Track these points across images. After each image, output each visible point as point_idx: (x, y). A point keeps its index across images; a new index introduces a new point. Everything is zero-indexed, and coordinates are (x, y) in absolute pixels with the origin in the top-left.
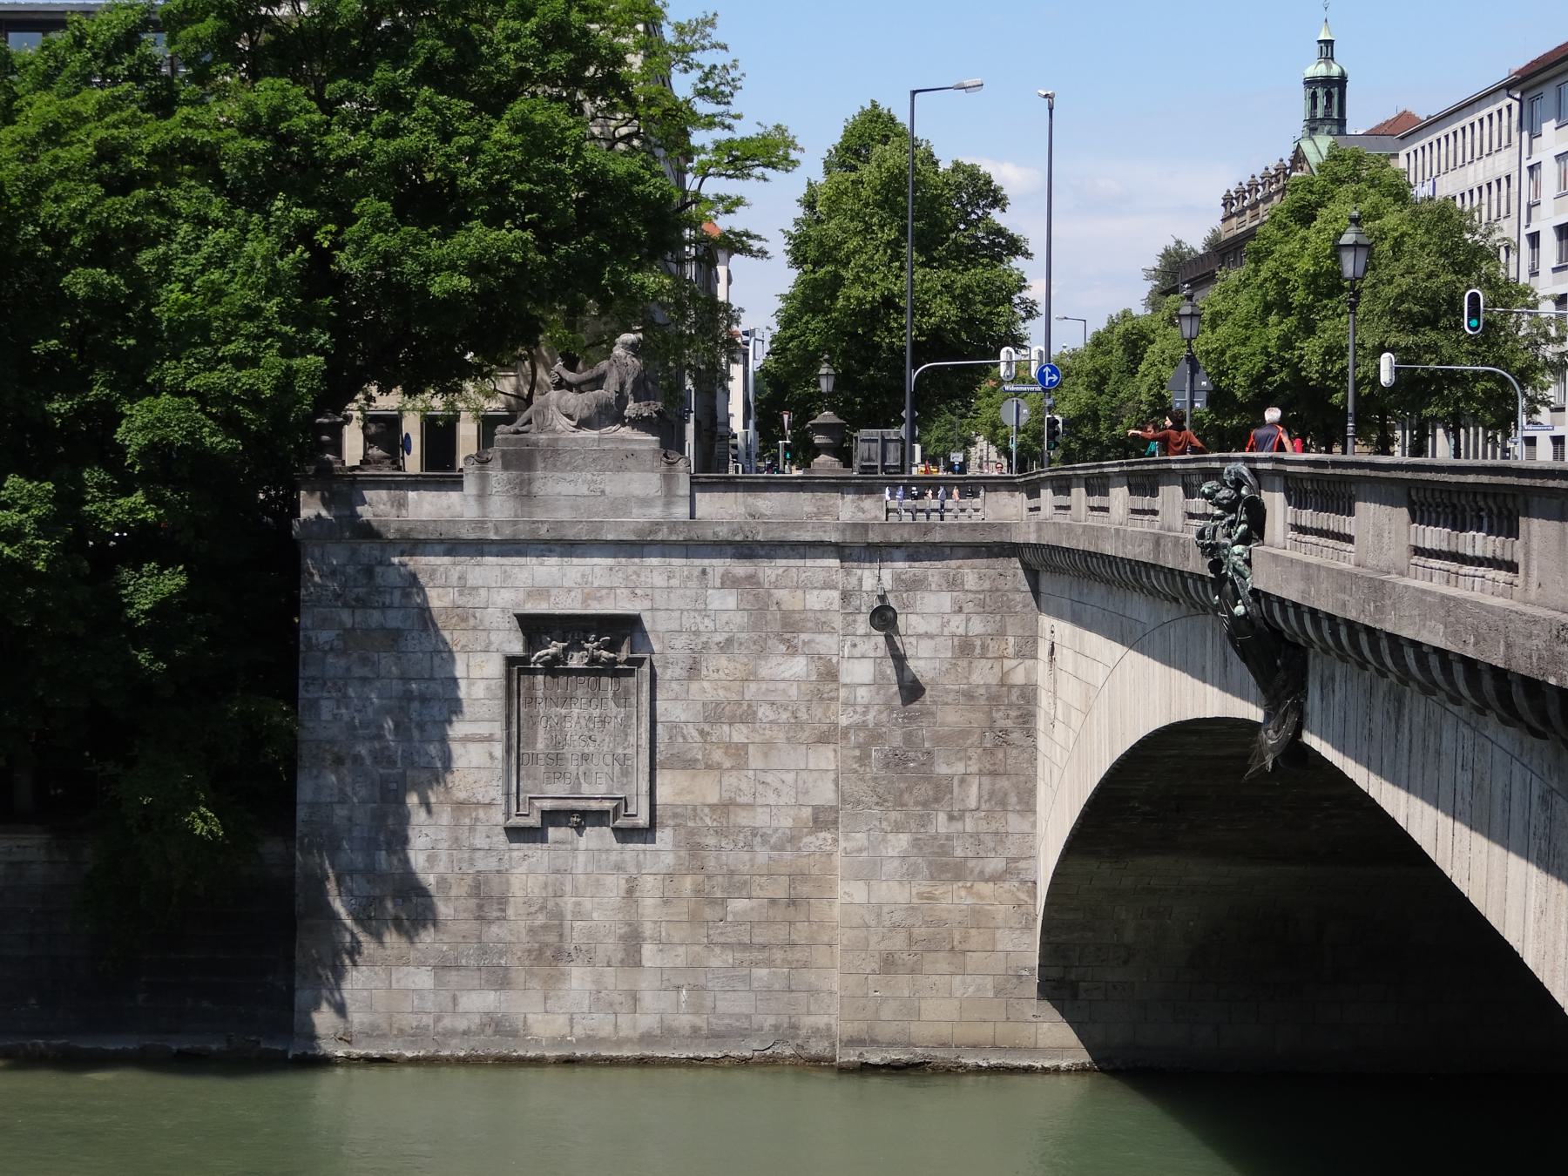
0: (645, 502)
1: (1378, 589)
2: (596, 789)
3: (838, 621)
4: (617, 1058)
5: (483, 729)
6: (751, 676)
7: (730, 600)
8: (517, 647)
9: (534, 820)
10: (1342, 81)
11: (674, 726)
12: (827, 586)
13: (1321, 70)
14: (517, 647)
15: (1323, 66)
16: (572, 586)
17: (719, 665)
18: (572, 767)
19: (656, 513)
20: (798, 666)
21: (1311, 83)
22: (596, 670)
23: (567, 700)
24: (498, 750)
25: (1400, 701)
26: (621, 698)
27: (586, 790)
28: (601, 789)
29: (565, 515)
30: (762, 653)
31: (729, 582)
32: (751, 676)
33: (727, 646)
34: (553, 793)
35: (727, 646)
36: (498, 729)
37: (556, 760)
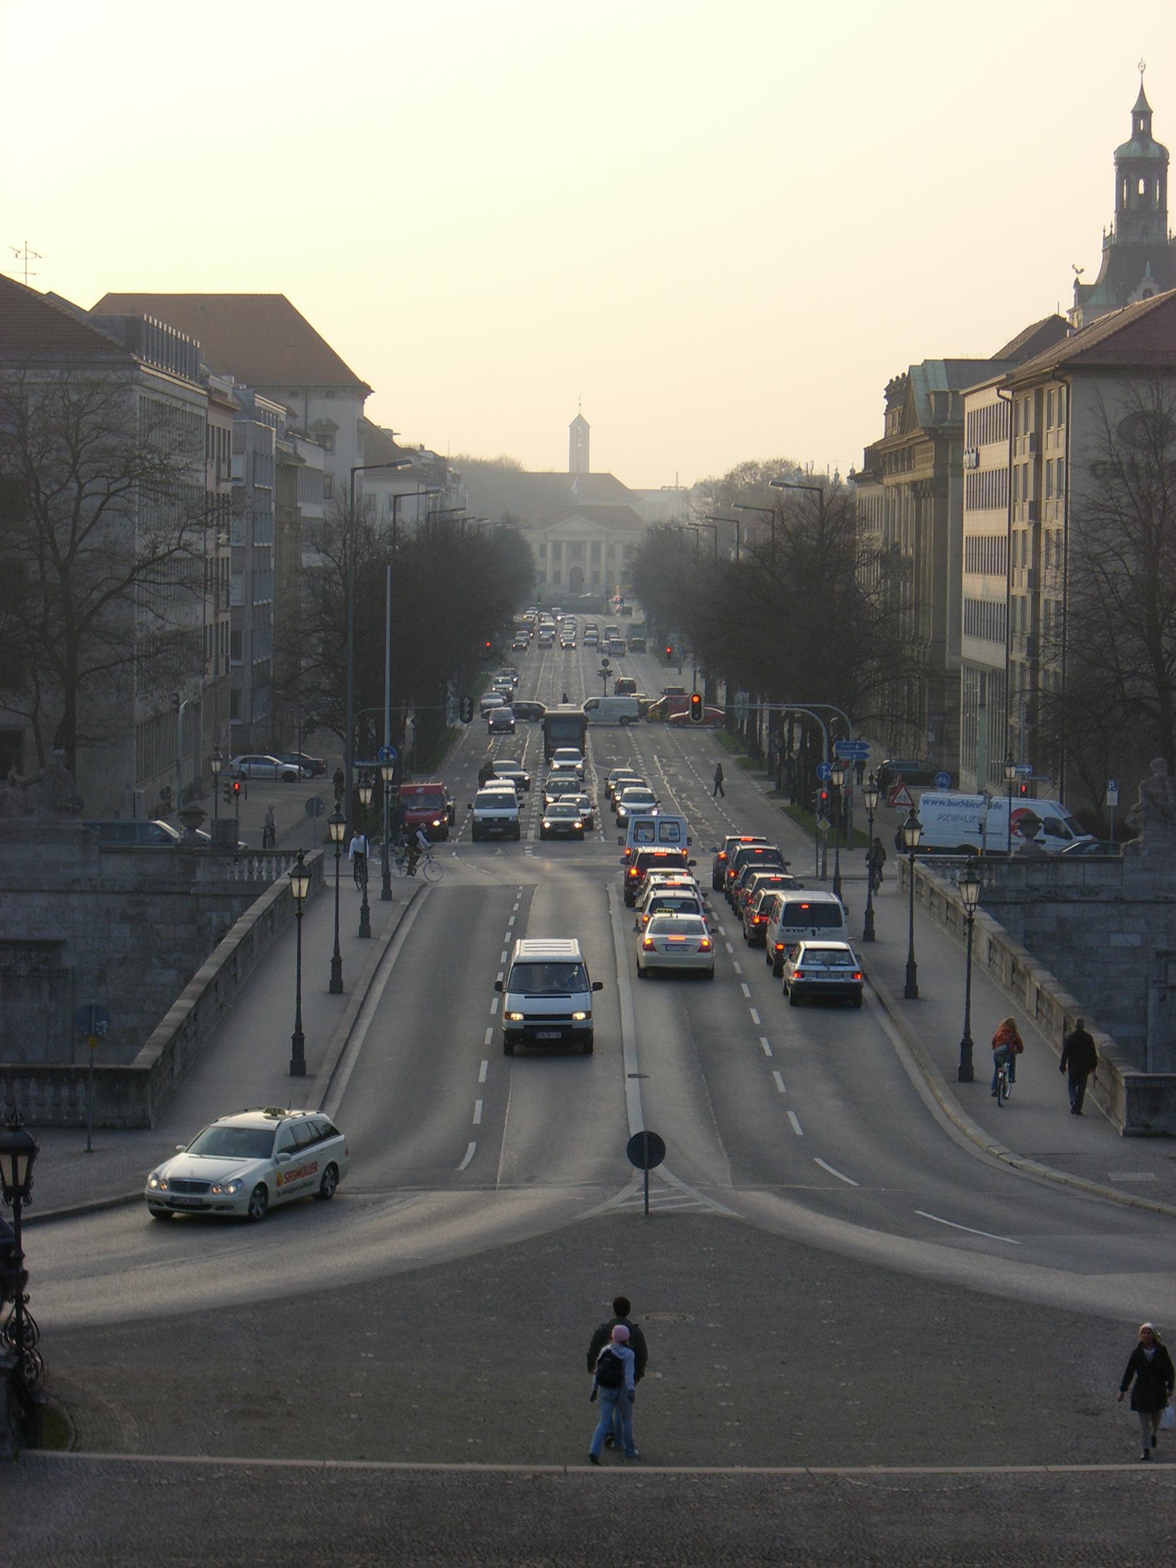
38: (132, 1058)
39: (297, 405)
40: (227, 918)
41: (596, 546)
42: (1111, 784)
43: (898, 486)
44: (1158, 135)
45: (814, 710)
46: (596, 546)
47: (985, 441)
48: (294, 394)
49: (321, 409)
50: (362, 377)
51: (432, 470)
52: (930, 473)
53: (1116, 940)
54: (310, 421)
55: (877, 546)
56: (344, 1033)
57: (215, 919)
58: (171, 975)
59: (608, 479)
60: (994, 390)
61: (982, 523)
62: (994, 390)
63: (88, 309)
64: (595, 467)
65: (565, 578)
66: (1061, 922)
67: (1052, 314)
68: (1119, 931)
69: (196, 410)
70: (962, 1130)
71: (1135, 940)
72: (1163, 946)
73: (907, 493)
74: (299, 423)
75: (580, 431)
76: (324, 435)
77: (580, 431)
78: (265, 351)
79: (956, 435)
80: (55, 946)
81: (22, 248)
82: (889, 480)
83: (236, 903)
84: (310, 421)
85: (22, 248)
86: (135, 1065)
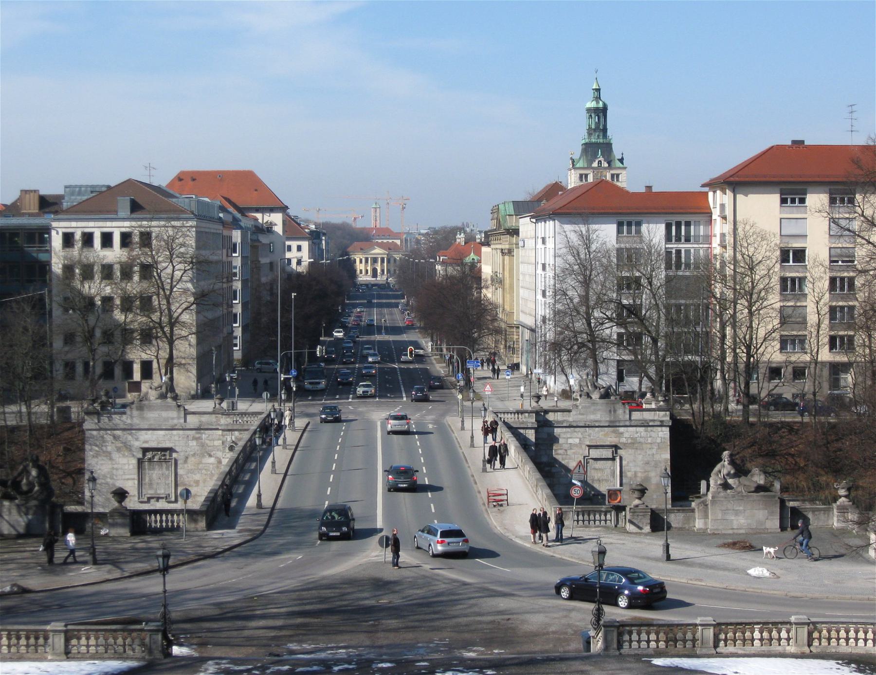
0: (173, 419)
1: (221, 473)
2: (161, 492)
3: (221, 448)
4: (305, 617)
5: (132, 477)
6: (200, 463)
7: (194, 443)
8: (140, 456)
9: (146, 499)
10: (604, 110)
11: (181, 475)
12: (219, 439)
13: (592, 104)
14: (140, 456)
15: (594, 102)
16: (152, 439)
17: (192, 460)
18: (155, 486)
19: (175, 421)
20: (212, 460)
21: (589, 110)
22: (160, 461)
23: (154, 469)
24: (136, 482)
25: (13, 526)
26: (167, 469)
27: (159, 492)
28: (162, 491)
29: (152, 422)
30: (203, 456)
31: (194, 438)
32: (200, 463)
33: (194, 455)
34: (150, 492)
35: (194, 455)
36: (136, 477)
37: (151, 484)
53: (570, 441)
71: (577, 441)
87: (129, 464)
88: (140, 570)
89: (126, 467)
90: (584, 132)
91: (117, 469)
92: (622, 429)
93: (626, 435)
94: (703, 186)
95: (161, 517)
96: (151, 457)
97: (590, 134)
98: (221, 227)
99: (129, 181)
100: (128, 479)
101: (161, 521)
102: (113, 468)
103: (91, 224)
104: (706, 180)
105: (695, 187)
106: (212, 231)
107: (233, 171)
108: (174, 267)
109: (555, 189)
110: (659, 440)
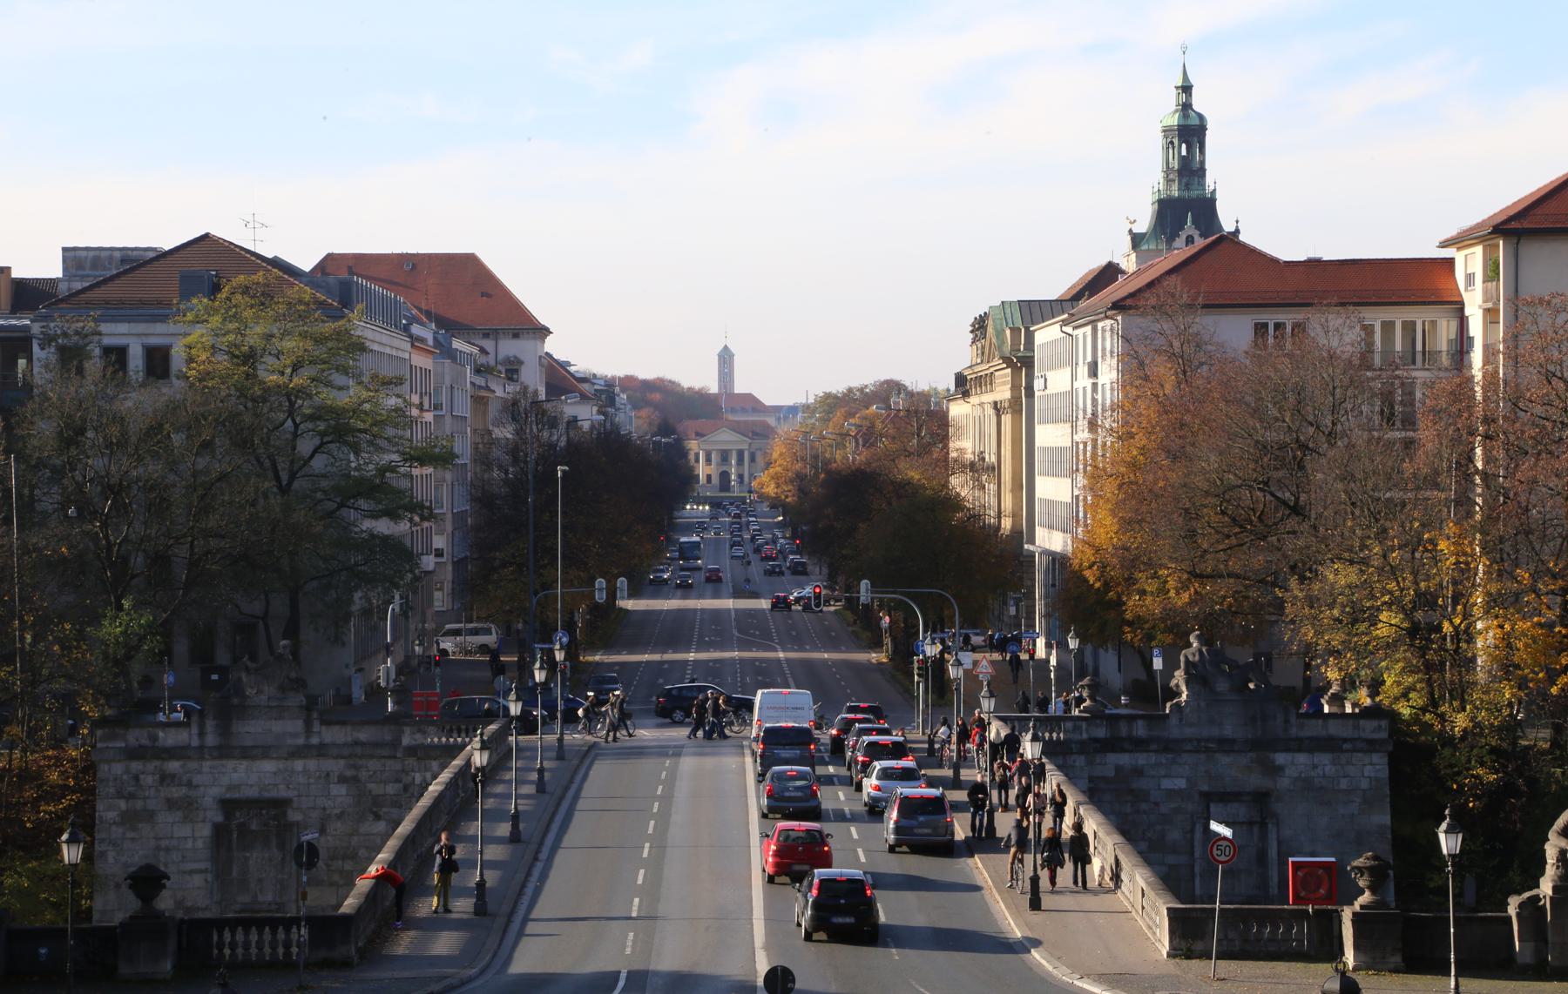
0: (295, 735)
14: (219, 818)
27: (260, 898)
28: (269, 898)
33: (340, 816)
38: (340, 905)
39: (488, 344)
40: (428, 775)
41: (740, 454)
42: (1156, 652)
43: (981, 404)
44: (1198, 106)
45: (908, 595)
46: (740, 454)
47: (1051, 368)
48: (486, 335)
49: (508, 348)
50: (543, 320)
51: (605, 392)
52: (1007, 395)
53: (1167, 784)
54: (500, 357)
55: (969, 456)
56: (520, 876)
57: (418, 778)
58: (381, 826)
59: (749, 398)
60: (1057, 326)
61: (1050, 436)
62: (1057, 326)
63: (307, 269)
64: (739, 388)
65: (715, 480)
66: (1118, 769)
67: (1104, 262)
68: (1167, 776)
69: (400, 354)
70: (1103, 869)
71: (1181, 783)
72: (1205, 788)
73: (990, 411)
74: (491, 360)
75: (726, 359)
76: (512, 370)
77: (726, 359)
78: (459, 299)
79: (1028, 363)
80: (281, 804)
81: (250, 219)
82: (974, 400)
83: (435, 765)
84: (500, 357)
85: (250, 219)
86: (343, 910)
87: (195, 839)
88: (910, 897)
89: (189, 845)
90: (1158, 176)
91: (167, 850)
92: (1280, 758)
93: (1291, 772)
94: (1445, 244)
95: (233, 935)
96: (248, 823)
97: (1168, 181)
98: (408, 346)
99: (206, 237)
100: (192, 872)
101: (233, 946)
102: (158, 848)
103: (123, 328)
104: (1452, 232)
105: (1426, 248)
106: (388, 351)
107: (430, 256)
108: (296, 426)
109: (1109, 273)
110: (1364, 784)
